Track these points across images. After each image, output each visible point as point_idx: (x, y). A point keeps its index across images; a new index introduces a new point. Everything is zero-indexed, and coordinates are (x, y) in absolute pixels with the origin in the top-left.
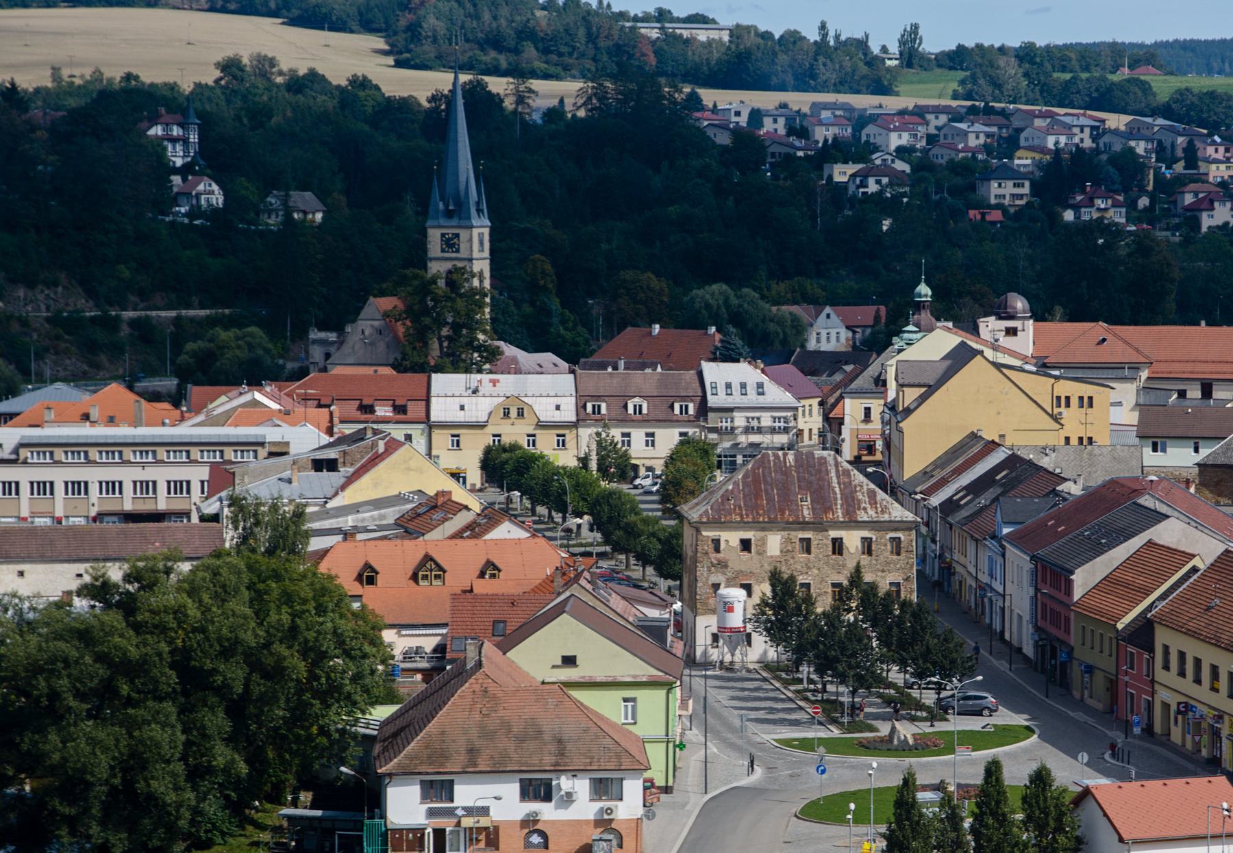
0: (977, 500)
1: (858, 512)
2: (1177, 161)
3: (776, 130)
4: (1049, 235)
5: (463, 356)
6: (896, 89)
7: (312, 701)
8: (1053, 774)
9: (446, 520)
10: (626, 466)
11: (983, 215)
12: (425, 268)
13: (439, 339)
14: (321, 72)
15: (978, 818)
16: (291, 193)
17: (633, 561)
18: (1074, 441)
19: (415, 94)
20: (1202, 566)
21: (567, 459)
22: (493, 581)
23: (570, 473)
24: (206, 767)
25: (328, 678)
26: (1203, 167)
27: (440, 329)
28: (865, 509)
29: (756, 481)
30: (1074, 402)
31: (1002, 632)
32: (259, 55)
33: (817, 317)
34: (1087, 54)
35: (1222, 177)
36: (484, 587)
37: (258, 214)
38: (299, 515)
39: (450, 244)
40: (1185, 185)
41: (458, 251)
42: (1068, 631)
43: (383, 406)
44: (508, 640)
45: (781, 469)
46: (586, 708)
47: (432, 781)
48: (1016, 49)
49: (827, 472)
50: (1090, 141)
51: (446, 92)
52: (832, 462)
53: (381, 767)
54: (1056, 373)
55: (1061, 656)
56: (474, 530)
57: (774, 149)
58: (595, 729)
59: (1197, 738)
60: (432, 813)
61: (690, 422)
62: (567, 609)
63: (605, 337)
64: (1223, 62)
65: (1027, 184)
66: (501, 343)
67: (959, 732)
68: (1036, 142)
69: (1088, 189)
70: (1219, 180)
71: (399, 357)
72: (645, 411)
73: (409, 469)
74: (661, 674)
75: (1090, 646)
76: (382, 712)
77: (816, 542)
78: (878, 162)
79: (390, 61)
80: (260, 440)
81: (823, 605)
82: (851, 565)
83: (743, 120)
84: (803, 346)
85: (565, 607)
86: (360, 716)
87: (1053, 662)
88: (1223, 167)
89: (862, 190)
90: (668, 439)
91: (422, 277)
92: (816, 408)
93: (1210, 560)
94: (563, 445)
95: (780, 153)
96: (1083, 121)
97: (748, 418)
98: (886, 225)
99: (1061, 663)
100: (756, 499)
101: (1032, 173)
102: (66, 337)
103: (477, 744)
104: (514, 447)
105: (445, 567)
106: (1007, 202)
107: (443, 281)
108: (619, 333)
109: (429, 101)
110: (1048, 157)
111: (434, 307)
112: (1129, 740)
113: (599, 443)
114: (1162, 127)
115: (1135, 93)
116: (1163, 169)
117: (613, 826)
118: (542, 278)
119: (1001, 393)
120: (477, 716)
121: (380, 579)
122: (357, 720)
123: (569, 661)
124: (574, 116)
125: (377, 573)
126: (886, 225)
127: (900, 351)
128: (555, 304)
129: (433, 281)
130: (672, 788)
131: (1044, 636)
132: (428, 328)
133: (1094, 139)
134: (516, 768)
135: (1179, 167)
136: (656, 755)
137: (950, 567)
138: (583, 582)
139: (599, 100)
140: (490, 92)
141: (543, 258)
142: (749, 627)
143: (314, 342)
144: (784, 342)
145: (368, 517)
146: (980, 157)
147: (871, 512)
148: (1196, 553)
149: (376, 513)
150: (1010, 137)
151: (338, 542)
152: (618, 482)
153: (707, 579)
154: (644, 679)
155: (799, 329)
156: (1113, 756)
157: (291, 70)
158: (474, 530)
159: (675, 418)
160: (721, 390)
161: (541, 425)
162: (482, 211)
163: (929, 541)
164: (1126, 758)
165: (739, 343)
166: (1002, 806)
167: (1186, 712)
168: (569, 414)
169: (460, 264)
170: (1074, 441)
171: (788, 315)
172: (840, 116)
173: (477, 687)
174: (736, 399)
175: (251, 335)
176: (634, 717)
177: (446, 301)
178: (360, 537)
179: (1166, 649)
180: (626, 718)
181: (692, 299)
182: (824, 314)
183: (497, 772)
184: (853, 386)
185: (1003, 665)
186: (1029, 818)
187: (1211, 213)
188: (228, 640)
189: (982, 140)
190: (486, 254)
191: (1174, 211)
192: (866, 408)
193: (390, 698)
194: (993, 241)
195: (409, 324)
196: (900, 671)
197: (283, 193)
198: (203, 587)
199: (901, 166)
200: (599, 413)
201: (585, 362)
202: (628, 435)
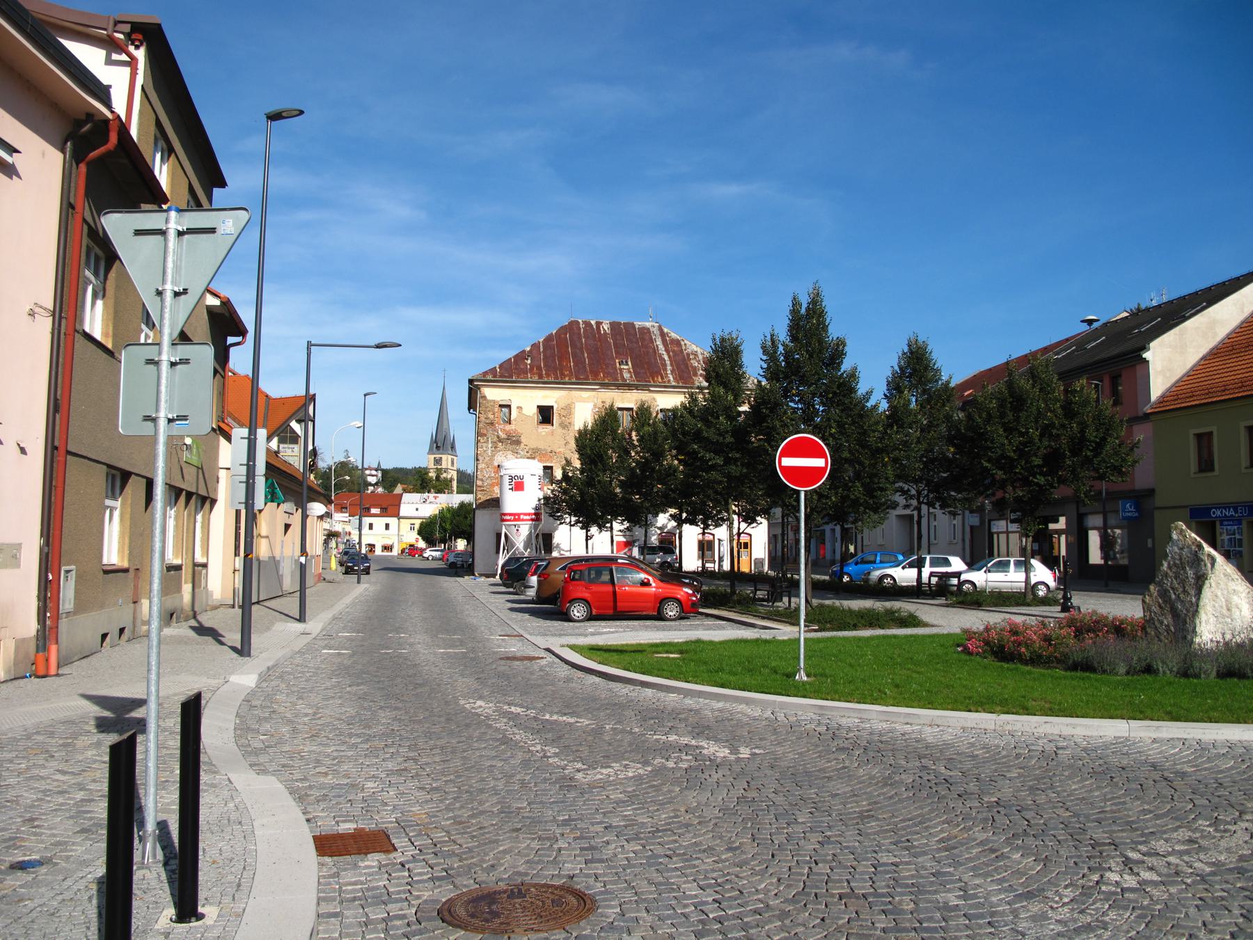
45: (594, 336)
49: (652, 341)
100: (561, 359)
102: (1226, 835)
131: (735, 598)
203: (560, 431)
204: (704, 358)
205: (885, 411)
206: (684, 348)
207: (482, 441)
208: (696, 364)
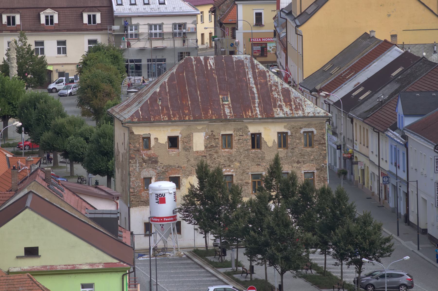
0: (376, 96)
1: (275, 110)
10: (42, 72)
28: (280, 107)
31: (407, 216)
49: (245, 74)
52: (249, 65)
61: (99, 29)
62: (28, 204)
72: (56, 21)
74: (115, 261)
77: (237, 138)
82: (270, 157)
85: (25, 203)
92: (207, 14)
113: (18, 50)
137: (351, 158)
138: (39, 180)
142: (179, 216)
147: (286, 109)
152: (34, 87)
153: (139, 173)
154: (101, 267)
159: (84, 27)
192: (257, 14)
203: (183, 153)
204: (282, 88)
205: (248, 257)
206: (268, 79)
207: (132, 162)
208: (276, 96)
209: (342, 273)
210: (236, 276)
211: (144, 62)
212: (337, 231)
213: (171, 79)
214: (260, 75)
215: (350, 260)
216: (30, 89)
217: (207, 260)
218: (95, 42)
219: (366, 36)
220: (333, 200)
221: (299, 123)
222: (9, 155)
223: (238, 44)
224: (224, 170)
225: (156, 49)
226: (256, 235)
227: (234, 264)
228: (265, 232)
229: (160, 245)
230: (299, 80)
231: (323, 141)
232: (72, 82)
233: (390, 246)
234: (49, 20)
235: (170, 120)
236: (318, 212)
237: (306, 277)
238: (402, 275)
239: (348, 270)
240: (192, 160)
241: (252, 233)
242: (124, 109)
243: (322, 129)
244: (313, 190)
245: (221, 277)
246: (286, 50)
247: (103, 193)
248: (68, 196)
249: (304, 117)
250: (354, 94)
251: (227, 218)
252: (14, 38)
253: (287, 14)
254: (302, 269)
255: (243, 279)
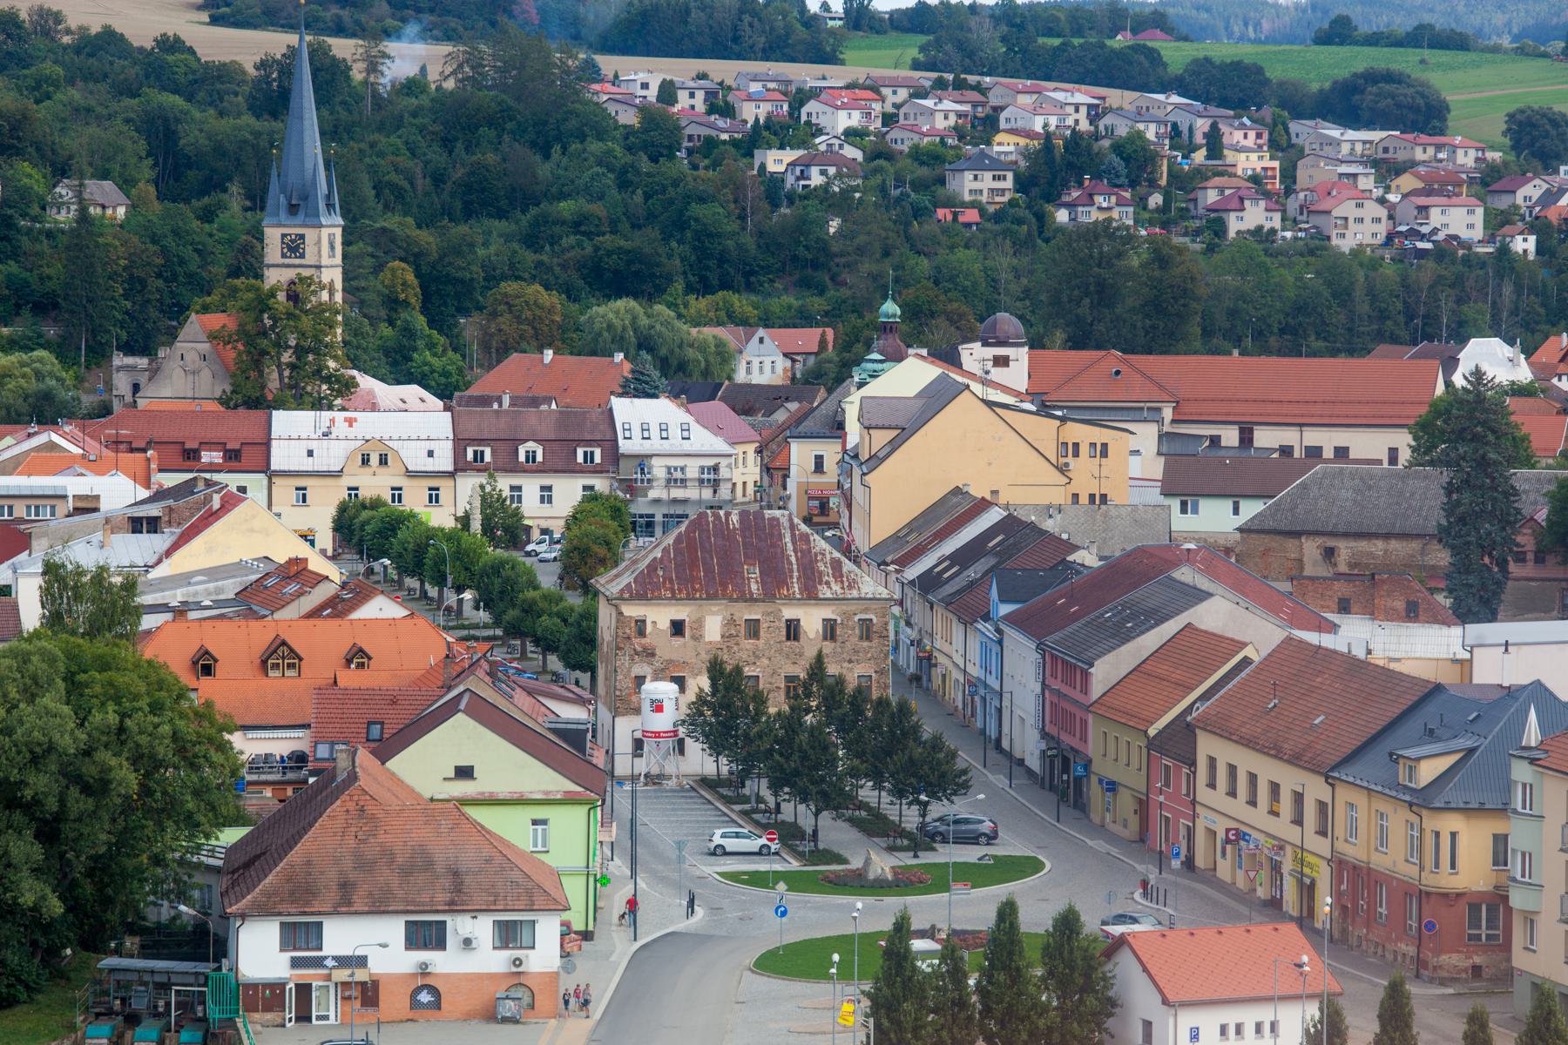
0: (965, 573)
2: (1195, 149)
3: (693, 107)
4: (1039, 241)
5: (309, 388)
6: (841, 56)
7: (143, 821)
8: (1082, 919)
9: (300, 594)
11: (955, 215)
12: (259, 276)
13: (279, 366)
14: (119, 30)
15: (988, 974)
16: (86, 182)
17: (530, 647)
18: (1084, 499)
19: (237, 58)
20: (1256, 658)
21: (441, 518)
22: (360, 672)
23: (450, 536)
24: (10, 905)
25: (165, 793)
26: (1230, 156)
27: (279, 355)
28: (828, 583)
29: (692, 547)
30: (1084, 450)
31: (999, 740)
32: (41, 8)
33: (747, 342)
34: (1079, 14)
35: (1254, 169)
36: (350, 678)
37: (44, 208)
38: (130, 586)
39: (294, 247)
40: (1207, 179)
41: (302, 256)
42: (1084, 739)
43: (210, 450)
44: (385, 749)
46: (489, 832)
47: (295, 923)
48: (990, 8)
49: (781, 536)
50: (1088, 122)
51: (278, 57)
52: (787, 524)
53: (231, 906)
54: (1059, 413)
55: (1075, 770)
56: (338, 607)
57: (692, 130)
58: (498, 859)
59: (1252, 874)
60: (296, 963)
61: (597, 471)
62: (462, 706)
63: (481, 366)
64: (1246, 24)
65: (1010, 175)
66: (355, 373)
67: (955, 863)
68: (1020, 124)
69: (1087, 183)
70: (1250, 172)
71: (228, 389)
72: (539, 458)
73: (252, 530)
75: (1125, 761)
76: (230, 836)
77: (766, 625)
78: (823, 148)
79: (205, 17)
80: (59, 493)
81: (777, 704)
82: (811, 653)
83: (652, 94)
84: (730, 378)
86: (203, 841)
87: (1065, 777)
88: (1254, 156)
89: (802, 182)
90: (569, 492)
91: (258, 289)
92: (751, 455)
93: (1265, 653)
94: (437, 501)
95: (699, 136)
96: (1080, 98)
97: (669, 468)
98: (834, 226)
99: (1075, 779)
100: (691, 570)
101: (1016, 162)
103: (352, 876)
104: (376, 504)
105: (302, 655)
106: (984, 198)
107: (284, 293)
108: (499, 362)
109: (257, 68)
110: (1036, 142)
111: (273, 328)
112: (1164, 875)
113: (483, 498)
114: (1177, 106)
115: (1141, 64)
116: (1179, 159)
117: (523, 980)
118: (403, 291)
119: (994, 438)
120: (352, 842)
121: (220, 670)
122: (199, 847)
123: (464, 773)
124: (439, 88)
125: (216, 661)
126: (834, 226)
127: (861, 385)
128: (420, 321)
129: (272, 294)
130: (592, 932)
132: (264, 353)
133: (1094, 118)
134: (401, 908)
135: (1199, 157)
136: (575, 890)
137: (929, 658)
139: (472, 68)
140: (334, 56)
141: (403, 265)
142: (682, 731)
143: (119, 369)
144: (706, 373)
145: (202, 591)
146: (950, 141)
147: (836, 587)
148: (1248, 640)
149: (211, 586)
150: (987, 116)
151: (167, 622)
152: (507, 548)
154: (559, 797)
155: (725, 356)
156: (1145, 895)
157: (80, 28)
158: (338, 607)
159: (578, 468)
160: (636, 432)
161: (411, 474)
162: (333, 206)
163: (903, 623)
164: (1161, 898)
165: (656, 374)
166: (1016, 958)
167: (1237, 840)
168: (444, 461)
169: (306, 273)
170: (1084, 499)
171: (711, 339)
172: (774, 90)
173: (351, 806)
174: (655, 445)
175: (40, 360)
176: (544, 845)
177: (288, 319)
178: (192, 615)
179: (1212, 762)
180: (535, 845)
181: (591, 320)
182: (756, 339)
183: (378, 908)
184: (800, 428)
185: (1000, 781)
186: (1051, 973)
187: (1240, 214)
188: (39, 744)
189: (952, 120)
190: (338, 260)
191: (1193, 212)
193: (237, 820)
194: (967, 247)
195: (242, 348)
196: (874, 788)
197: (77, 183)
198: (8, 678)
199: (852, 152)
200: (482, 460)
201: (461, 397)
202: (519, 488)
203: (692, 643)
209: (901, 816)
210: (755, 816)
211: (659, 518)
212: (895, 758)
213: (678, 540)
214: (801, 540)
215: (911, 798)
216: (498, 551)
217: (717, 792)
218: (591, 488)
219: (957, 491)
220: (892, 716)
221: (852, 607)
222: (449, 639)
223: (789, 497)
224: (746, 669)
225: (675, 501)
226: (782, 760)
227: (753, 799)
228: (796, 756)
229: (655, 770)
230: (865, 549)
231: (885, 633)
232: (558, 542)
233: (967, 781)
234: (531, 456)
235: (673, 597)
236: (872, 731)
237: (852, 821)
238: (981, 822)
239: (908, 812)
240: (703, 653)
241: (777, 757)
242: (612, 580)
243: (884, 616)
244: (867, 700)
245: (734, 817)
246: (849, 506)
247: (571, 695)
248: (520, 697)
249: (860, 599)
250: (937, 570)
251: (746, 735)
252: (482, 479)
253: (852, 457)
254: (847, 809)
255: (764, 821)
